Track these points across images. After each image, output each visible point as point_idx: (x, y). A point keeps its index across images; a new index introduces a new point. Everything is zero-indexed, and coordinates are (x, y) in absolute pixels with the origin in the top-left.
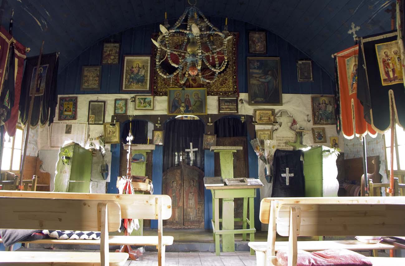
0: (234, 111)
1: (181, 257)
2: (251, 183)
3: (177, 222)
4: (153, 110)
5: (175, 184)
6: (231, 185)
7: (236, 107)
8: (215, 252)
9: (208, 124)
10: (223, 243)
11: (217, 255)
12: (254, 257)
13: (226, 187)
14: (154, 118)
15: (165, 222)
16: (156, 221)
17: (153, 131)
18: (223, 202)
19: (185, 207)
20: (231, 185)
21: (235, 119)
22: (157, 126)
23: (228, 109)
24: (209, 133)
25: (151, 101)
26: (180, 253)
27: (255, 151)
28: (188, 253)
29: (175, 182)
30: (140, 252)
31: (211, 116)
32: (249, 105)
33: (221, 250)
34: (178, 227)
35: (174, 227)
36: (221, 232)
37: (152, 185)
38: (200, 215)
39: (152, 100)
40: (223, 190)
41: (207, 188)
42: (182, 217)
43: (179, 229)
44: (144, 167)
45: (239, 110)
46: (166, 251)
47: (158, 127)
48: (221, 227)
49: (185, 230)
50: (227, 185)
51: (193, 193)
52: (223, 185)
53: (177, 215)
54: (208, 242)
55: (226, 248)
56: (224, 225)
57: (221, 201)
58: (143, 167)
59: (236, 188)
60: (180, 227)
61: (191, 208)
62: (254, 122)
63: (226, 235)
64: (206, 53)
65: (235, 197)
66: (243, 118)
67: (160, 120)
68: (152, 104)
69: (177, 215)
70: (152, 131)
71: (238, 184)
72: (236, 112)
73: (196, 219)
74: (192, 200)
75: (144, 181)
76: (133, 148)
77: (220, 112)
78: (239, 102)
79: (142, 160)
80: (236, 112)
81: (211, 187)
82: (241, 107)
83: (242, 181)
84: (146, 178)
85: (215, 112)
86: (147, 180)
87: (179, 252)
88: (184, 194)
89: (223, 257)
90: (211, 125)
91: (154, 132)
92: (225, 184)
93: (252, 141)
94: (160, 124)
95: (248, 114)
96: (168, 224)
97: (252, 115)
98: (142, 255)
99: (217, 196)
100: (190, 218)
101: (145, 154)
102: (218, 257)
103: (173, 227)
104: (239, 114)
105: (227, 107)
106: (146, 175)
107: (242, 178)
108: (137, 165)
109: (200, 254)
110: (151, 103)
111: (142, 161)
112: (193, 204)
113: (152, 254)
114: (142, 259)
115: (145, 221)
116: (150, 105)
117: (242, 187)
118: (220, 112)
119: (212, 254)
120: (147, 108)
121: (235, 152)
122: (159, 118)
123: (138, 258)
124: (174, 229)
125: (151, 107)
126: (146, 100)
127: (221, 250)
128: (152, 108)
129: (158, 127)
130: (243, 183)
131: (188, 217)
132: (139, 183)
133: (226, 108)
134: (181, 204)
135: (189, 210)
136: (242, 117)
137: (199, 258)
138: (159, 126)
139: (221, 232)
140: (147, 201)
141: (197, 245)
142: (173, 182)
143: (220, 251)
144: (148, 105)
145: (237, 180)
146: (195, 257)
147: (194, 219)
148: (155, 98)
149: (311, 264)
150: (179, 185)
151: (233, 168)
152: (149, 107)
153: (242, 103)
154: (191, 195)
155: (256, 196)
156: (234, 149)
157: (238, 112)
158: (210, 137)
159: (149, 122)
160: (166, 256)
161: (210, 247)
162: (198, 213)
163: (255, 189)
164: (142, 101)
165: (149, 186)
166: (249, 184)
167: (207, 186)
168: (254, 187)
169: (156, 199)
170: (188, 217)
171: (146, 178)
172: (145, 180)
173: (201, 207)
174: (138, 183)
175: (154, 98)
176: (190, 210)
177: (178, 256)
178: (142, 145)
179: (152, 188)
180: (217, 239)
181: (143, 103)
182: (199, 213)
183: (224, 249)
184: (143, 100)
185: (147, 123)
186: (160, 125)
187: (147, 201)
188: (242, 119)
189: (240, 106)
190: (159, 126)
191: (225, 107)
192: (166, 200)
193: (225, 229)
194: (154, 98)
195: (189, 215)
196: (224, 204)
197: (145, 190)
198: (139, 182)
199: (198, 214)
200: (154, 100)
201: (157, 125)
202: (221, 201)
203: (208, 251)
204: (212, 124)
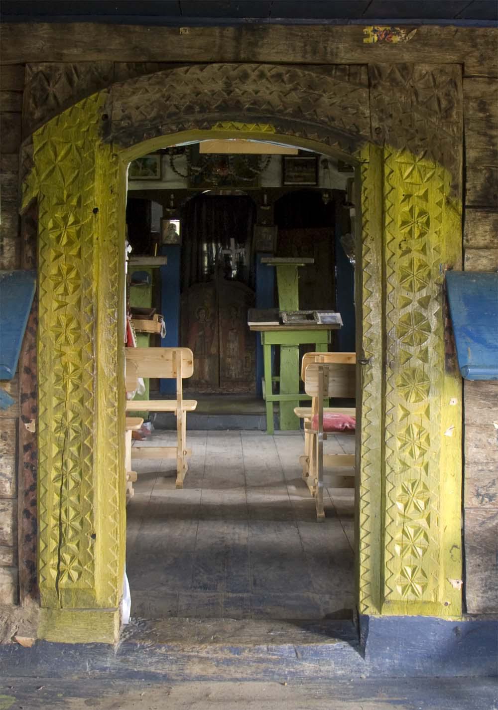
0: (311, 182)
1: (211, 436)
2: (324, 320)
3: (206, 381)
4: (160, 180)
5: (202, 315)
6: (291, 325)
7: (314, 175)
8: (266, 430)
9: (262, 207)
10: (281, 416)
11: (269, 434)
12: (258, 414)
13: (282, 327)
14: (163, 196)
15: (185, 381)
16: (173, 381)
17: (162, 219)
18: (281, 348)
19: (221, 356)
20: (291, 325)
21: (311, 196)
22: (169, 212)
23: (299, 179)
24: (265, 223)
25: (156, 163)
26: (210, 432)
27: (348, 256)
28: (223, 432)
29: (204, 311)
30: (146, 429)
31: (269, 191)
32: (339, 171)
33: (277, 426)
34: (209, 390)
35: (203, 392)
36: (276, 398)
37: (163, 323)
38: (249, 369)
39: (158, 162)
40: (277, 331)
41: (251, 329)
42: (217, 373)
43: (210, 394)
44: (149, 292)
45: (321, 181)
46: (187, 429)
47: (171, 213)
48: (276, 389)
49: (222, 397)
50: (284, 324)
51: (235, 331)
52: (277, 323)
53: (207, 369)
54: (258, 414)
55: (285, 424)
56: (282, 387)
57: (276, 349)
58: (148, 293)
59: (296, 328)
60: (213, 392)
61: (232, 357)
62: (345, 205)
63: (286, 402)
64: (251, 106)
65: (302, 343)
66: (327, 196)
67: (173, 200)
68: (158, 170)
69: (207, 369)
70: (159, 219)
71: (301, 322)
72: (315, 183)
73: (241, 377)
74: (233, 342)
75: (151, 318)
76: (131, 264)
77: (286, 183)
78: (320, 165)
79: (145, 281)
80: (315, 183)
81: (258, 328)
82: (324, 174)
83: (310, 317)
84: (153, 312)
85: (276, 184)
86: (156, 316)
87: (208, 430)
88: (221, 333)
89: (278, 437)
90: (267, 210)
91: (164, 221)
92: (281, 323)
93: (342, 238)
94: (174, 208)
95: (337, 188)
96: (191, 386)
97: (345, 189)
98: (150, 433)
99: (269, 340)
100: (231, 375)
101: (150, 272)
102: (271, 437)
103: (200, 392)
104: (321, 187)
105: (297, 174)
106: (153, 305)
107: (310, 312)
108: (138, 290)
109: (242, 433)
110: (156, 167)
111: (147, 283)
112: (236, 349)
113: (166, 433)
114: (150, 439)
115: (151, 380)
116: (155, 172)
117: (306, 327)
118: (286, 183)
119: (262, 433)
120: (151, 177)
121: (302, 267)
122: (172, 196)
123: (145, 437)
124: (203, 394)
125: (156, 175)
126: (148, 162)
127: (277, 426)
128: (158, 177)
129: (171, 213)
130: (310, 321)
131: (227, 373)
132: (143, 321)
133: (296, 177)
134: (214, 350)
135: (229, 360)
136: (324, 195)
137: (239, 438)
138: (173, 213)
139: (276, 398)
140: (162, 356)
141: (238, 419)
142: (200, 310)
143: (273, 429)
144: (151, 172)
145: (303, 315)
146: (233, 436)
147: (237, 377)
148: (163, 159)
149: (344, 427)
150: (210, 315)
151: (298, 293)
152: (154, 174)
153: (326, 167)
154: (232, 334)
155: (330, 342)
156: (301, 262)
157: (317, 185)
158: (265, 229)
159: (153, 203)
160: (187, 435)
161: (259, 423)
162: (246, 367)
163: (328, 330)
164: (140, 165)
165: (159, 324)
166: (319, 323)
167: (252, 326)
168: (327, 327)
169: (174, 353)
170: (227, 373)
171: (153, 312)
172: (152, 316)
173: (249, 354)
174: (141, 320)
175: (161, 158)
176: (230, 360)
177: (207, 435)
178: (145, 258)
179: (164, 329)
180: (269, 407)
181: (142, 168)
182: (248, 366)
183: (282, 425)
184: (142, 162)
185: (150, 202)
186: (174, 210)
187: (162, 356)
188: (325, 198)
189: (321, 172)
190: (173, 213)
191: (294, 174)
192: (185, 355)
193: (284, 393)
194: (161, 158)
195: (229, 369)
196: (284, 355)
197: (153, 332)
198: (142, 319)
199: (244, 368)
200: (161, 161)
201: (168, 210)
202: (276, 349)
203: (256, 429)
204: (268, 208)
